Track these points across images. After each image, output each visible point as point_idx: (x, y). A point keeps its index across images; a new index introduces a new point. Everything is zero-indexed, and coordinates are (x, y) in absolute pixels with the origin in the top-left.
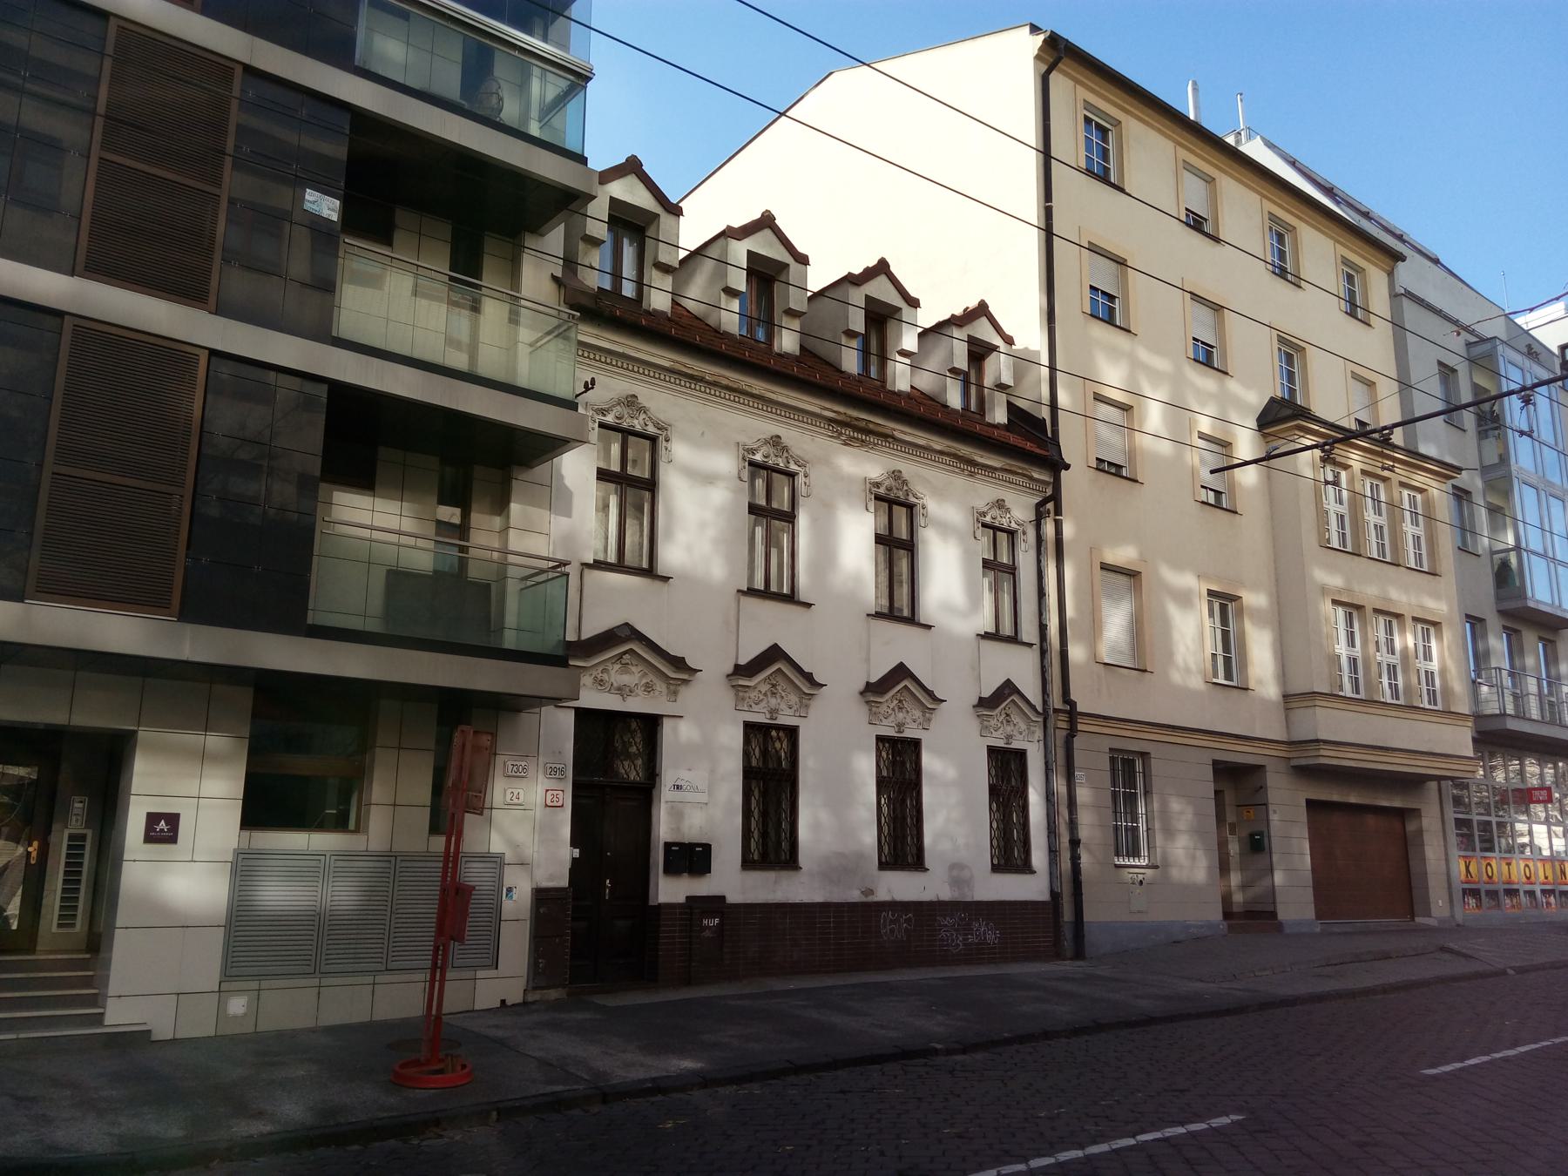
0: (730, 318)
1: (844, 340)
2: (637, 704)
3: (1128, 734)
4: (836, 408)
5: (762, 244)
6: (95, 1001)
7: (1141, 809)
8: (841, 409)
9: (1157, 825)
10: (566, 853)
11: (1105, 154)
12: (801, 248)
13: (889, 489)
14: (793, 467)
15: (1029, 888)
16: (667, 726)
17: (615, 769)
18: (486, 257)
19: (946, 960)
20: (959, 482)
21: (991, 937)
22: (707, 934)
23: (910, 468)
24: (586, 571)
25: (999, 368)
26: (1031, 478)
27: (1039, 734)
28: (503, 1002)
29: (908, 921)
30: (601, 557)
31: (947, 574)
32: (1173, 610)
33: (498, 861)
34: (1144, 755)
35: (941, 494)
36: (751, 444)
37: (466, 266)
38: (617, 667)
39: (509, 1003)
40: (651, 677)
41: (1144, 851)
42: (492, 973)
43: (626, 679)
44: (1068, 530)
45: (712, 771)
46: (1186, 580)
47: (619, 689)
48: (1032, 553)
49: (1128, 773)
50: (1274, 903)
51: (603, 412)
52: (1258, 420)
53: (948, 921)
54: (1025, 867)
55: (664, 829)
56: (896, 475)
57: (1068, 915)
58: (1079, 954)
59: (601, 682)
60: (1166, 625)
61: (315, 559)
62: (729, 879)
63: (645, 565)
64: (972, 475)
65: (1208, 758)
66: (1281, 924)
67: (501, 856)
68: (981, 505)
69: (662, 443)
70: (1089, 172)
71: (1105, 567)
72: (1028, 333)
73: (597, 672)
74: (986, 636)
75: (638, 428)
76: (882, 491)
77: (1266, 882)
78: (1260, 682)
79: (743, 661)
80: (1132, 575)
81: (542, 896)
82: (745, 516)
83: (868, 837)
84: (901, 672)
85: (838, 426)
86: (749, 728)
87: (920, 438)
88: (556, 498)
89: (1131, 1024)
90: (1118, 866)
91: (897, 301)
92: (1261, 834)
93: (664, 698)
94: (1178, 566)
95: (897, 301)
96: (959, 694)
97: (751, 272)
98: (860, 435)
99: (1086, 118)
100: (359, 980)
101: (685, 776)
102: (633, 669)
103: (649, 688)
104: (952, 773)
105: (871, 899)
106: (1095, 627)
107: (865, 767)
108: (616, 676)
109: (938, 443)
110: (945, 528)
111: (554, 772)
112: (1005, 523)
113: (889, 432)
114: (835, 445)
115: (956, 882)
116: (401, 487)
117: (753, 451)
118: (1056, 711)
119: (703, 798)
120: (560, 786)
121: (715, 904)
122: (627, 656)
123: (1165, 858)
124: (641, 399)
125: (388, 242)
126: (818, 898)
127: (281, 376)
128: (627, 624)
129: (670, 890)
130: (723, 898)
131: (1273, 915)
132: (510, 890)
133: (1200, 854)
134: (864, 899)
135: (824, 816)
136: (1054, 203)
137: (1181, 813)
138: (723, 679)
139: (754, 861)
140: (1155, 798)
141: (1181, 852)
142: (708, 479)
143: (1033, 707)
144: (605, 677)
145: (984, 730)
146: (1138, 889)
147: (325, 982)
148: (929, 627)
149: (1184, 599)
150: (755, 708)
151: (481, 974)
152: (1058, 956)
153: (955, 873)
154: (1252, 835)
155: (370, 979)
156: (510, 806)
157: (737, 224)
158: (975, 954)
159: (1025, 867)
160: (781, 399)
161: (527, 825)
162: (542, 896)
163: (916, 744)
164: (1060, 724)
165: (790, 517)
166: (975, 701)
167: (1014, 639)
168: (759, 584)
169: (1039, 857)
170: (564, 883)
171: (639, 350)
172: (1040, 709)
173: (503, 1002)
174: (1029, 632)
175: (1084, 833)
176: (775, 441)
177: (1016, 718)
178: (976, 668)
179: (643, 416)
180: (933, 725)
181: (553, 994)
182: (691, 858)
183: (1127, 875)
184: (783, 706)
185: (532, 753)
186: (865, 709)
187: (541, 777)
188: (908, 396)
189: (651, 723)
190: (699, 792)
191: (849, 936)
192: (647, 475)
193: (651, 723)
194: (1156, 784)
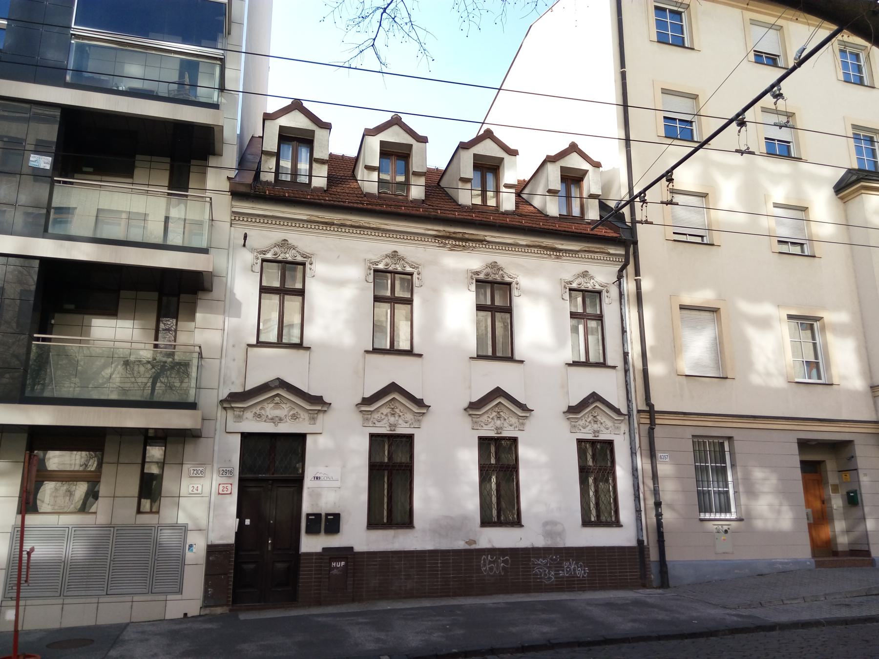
0: (553, 208)
1: (460, 185)
3: (735, 425)
4: (436, 228)
5: (393, 136)
7: (730, 478)
8: (441, 228)
9: (741, 489)
10: (233, 523)
11: (859, 69)
12: (595, 158)
13: (487, 275)
14: (408, 269)
16: (309, 439)
17: (272, 467)
18: (191, 175)
20: (549, 263)
21: (580, 572)
22: (335, 572)
23: (295, 237)
24: (249, 349)
25: (592, 184)
26: (609, 254)
27: (624, 427)
28: (185, 614)
29: (505, 562)
30: (576, 360)
31: (540, 325)
32: (752, 333)
33: (184, 529)
34: (730, 439)
36: (375, 258)
37: (179, 183)
38: (271, 405)
39: (189, 615)
40: (297, 410)
41: (733, 509)
42: (178, 597)
43: (278, 413)
44: (646, 285)
45: (344, 467)
46: (767, 309)
47: (272, 419)
48: (616, 305)
49: (712, 453)
50: (868, 544)
52: (835, 188)
53: (541, 561)
54: (617, 524)
55: (307, 507)
56: (494, 265)
57: (654, 555)
58: (664, 583)
59: (259, 416)
60: (746, 344)
62: (357, 535)
63: (602, 361)
64: (558, 257)
65: (793, 438)
66: (873, 560)
68: (568, 277)
69: (308, 266)
70: (845, 81)
71: (683, 307)
72: (612, 158)
73: (257, 410)
74: (576, 364)
75: (290, 259)
76: (482, 276)
77: (860, 528)
78: (844, 378)
79: (367, 395)
80: (715, 311)
81: (212, 550)
82: (568, 322)
83: (472, 505)
84: (594, 397)
86: (484, 442)
87: (508, 238)
88: (232, 307)
89: (682, 636)
90: (702, 520)
91: (499, 153)
92: (855, 492)
93: (307, 422)
94: (756, 298)
95: (499, 153)
97: (476, 167)
98: (462, 243)
99: (656, 8)
100: (89, 600)
101: (321, 470)
102: (284, 406)
103: (295, 417)
104: (543, 458)
105: (473, 547)
106: (674, 349)
107: (469, 459)
108: (270, 410)
109: (523, 240)
110: (535, 295)
111: (226, 473)
112: (590, 286)
113: (481, 238)
114: (444, 251)
115: (548, 534)
116: (133, 313)
117: (376, 263)
118: (639, 411)
119: (338, 484)
120: (230, 481)
121: (346, 553)
122: (277, 399)
123: (748, 512)
124: (290, 241)
125: (131, 175)
126: (429, 546)
127: (10, 259)
128: (278, 379)
129: (310, 544)
130: (352, 548)
131: (867, 553)
132: (191, 546)
133: (785, 509)
134: (467, 547)
135: (433, 492)
136: (628, 69)
137: (765, 479)
138: (353, 407)
139: (384, 524)
140: (739, 469)
141: (768, 508)
142: (341, 283)
143: (617, 411)
144: (263, 412)
145: (573, 429)
146: (724, 537)
147: (66, 601)
148: (522, 362)
149: (764, 323)
150: (378, 424)
151: (169, 597)
152: (644, 583)
153: (548, 528)
154: (848, 493)
155: (95, 600)
156: (191, 495)
157: (553, 154)
158: (570, 584)
159: (617, 524)
160: (392, 228)
161: (204, 506)
162: (212, 550)
163: (514, 441)
164: (643, 421)
165: (409, 302)
166: (566, 409)
167: (603, 365)
168: (271, 336)
169: (626, 514)
170: (231, 540)
171: (283, 212)
172: (624, 410)
173: (185, 614)
174: (614, 358)
175: (666, 496)
176: (394, 255)
177: (601, 418)
178: (564, 386)
179: (294, 251)
180: (526, 428)
181: (219, 610)
182: (331, 523)
183: (711, 526)
184: (400, 421)
185: (205, 462)
186: (469, 419)
187: (215, 476)
188: (380, 196)
189: (301, 438)
190: (335, 478)
191: (453, 571)
192: (598, 312)
193: (301, 438)
194: (738, 457)
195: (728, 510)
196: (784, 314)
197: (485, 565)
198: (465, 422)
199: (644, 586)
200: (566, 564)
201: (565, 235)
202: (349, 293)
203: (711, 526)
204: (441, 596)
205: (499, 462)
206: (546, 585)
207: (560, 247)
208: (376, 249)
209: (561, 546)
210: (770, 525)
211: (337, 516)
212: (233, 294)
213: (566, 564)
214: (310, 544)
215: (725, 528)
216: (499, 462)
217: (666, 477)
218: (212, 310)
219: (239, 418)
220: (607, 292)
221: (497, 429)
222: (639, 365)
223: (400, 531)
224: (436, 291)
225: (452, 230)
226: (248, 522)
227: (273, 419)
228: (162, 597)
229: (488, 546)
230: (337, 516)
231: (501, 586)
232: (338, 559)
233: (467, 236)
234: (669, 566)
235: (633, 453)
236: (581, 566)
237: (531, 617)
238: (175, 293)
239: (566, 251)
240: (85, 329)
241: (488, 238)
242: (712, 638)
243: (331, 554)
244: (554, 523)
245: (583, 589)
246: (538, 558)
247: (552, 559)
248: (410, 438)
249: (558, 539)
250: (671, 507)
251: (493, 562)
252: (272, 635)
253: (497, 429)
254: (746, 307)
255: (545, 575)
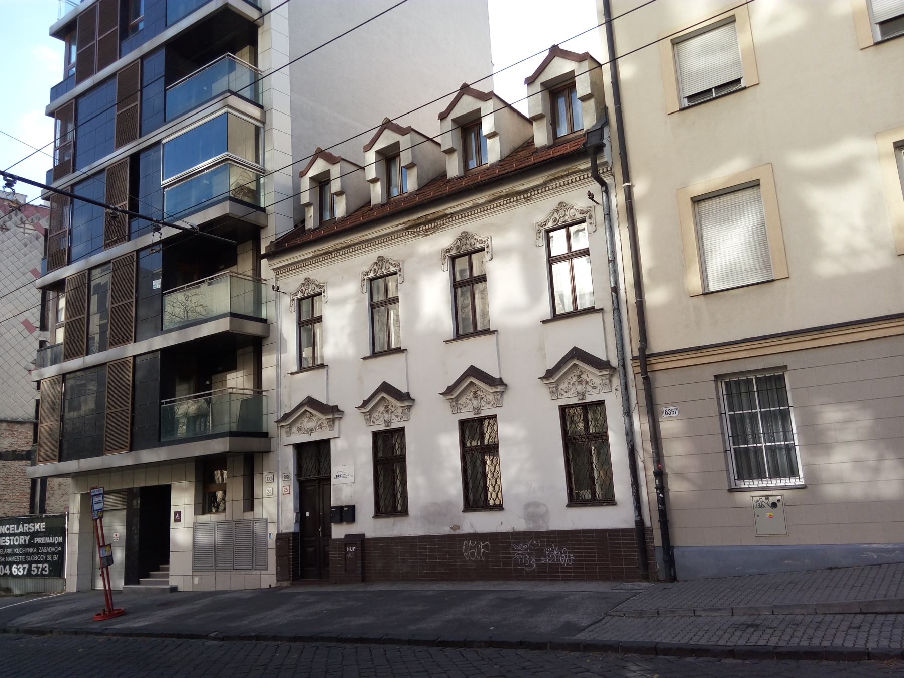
2: (316, 437)
4: (402, 221)
6: (168, 576)
8: (406, 220)
15: (617, 517)
19: (521, 575)
21: (565, 559)
23: (471, 225)
26: (580, 171)
27: (616, 382)
29: (486, 547)
33: (265, 521)
35: (501, 228)
44: (639, 189)
51: (296, 294)
53: (521, 547)
54: (609, 500)
60: (808, 218)
61: (264, 417)
62: (368, 525)
64: (528, 199)
65: (709, 373)
67: (266, 520)
68: (541, 218)
75: (312, 293)
81: (280, 537)
84: (576, 354)
85: (412, 228)
96: (522, 370)
98: (430, 225)
107: (450, 444)
109: (481, 198)
111: (286, 478)
115: (531, 517)
121: (359, 540)
126: (420, 532)
129: (339, 532)
134: (452, 532)
145: (555, 392)
146: (770, 512)
149: (844, 173)
150: (377, 423)
153: (531, 509)
158: (551, 573)
159: (609, 500)
161: (276, 504)
172: (614, 362)
175: (672, 464)
182: (347, 514)
184: (393, 417)
190: (352, 477)
191: (441, 556)
193: (327, 442)
195: (793, 473)
196: (887, 143)
197: (466, 551)
198: (543, 392)
199: (646, 578)
200: (548, 550)
201: (516, 175)
202: (349, 308)
203: (746, 497)
204: (431, 580)
205: (478, 445)
206: (527, 573)
207: (521, 188)
208: (362, 261)
209: (544, 529)
210: (857, 492)
211: (352, 508)
212: (281, 334)
213: (548, 550)
214: (339, 532)
215: (773, 499)
216: (478, 445)
217: (674, 438)
218: (270, 352)
219: (289, 433)
220: (590, 218)
221: (474, 409)
222: (632, 298)
223: (398, 519)
224: (414, 282)
225: (415, 217)
226: (308, 514)
227: (310, 431)
228: (258, 573)
229: (471, 531)
230: (352, 508)
231: (484, 572)
232: (351, 545)
233: (429, 217)
234: (676, 553)
235: (628, 414)
236: (565, 553)
237: (482, 604)
238: (242, 345)
239: (533, 189)
240: (224, 380)
241: (448, 212)
242: (825, 663)
243: (350, 539)
244: (536, 504)
245: (566, 579)
246: (518, 543)
247: (532, 544)
248: (402, 430)
249: (541, 522)
250: (681, 475)
251: (474, 548)
252: (315, 604)
253: (474, 409)
254: (803, 160)
255: (526, 561)
